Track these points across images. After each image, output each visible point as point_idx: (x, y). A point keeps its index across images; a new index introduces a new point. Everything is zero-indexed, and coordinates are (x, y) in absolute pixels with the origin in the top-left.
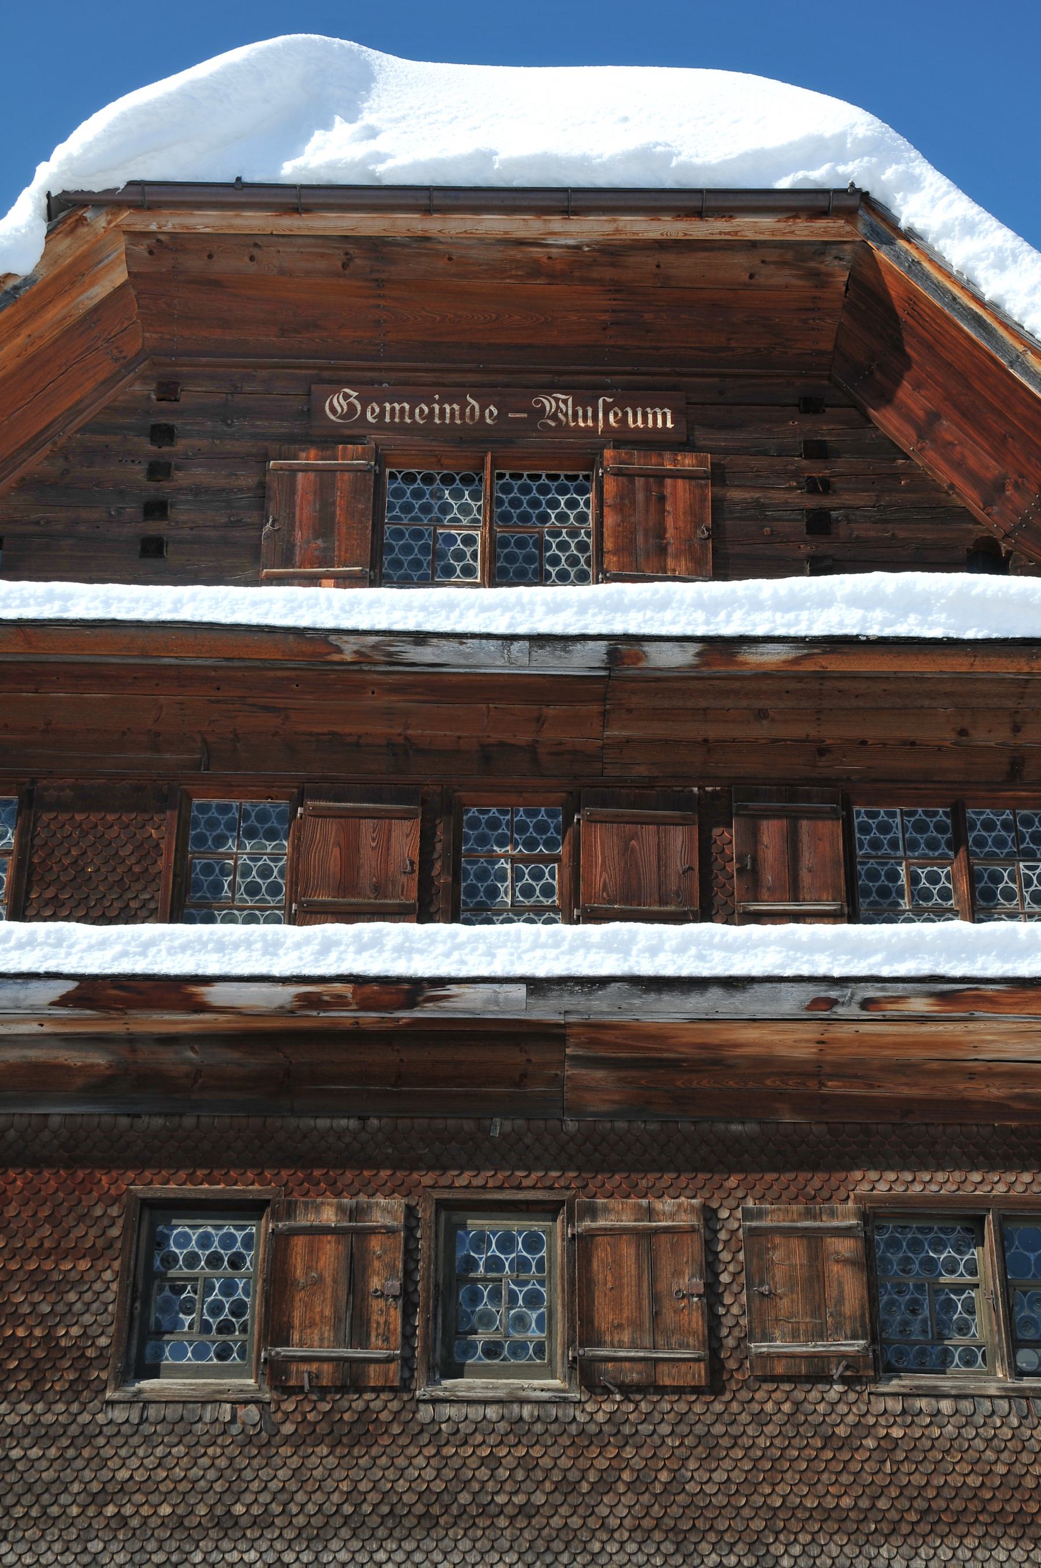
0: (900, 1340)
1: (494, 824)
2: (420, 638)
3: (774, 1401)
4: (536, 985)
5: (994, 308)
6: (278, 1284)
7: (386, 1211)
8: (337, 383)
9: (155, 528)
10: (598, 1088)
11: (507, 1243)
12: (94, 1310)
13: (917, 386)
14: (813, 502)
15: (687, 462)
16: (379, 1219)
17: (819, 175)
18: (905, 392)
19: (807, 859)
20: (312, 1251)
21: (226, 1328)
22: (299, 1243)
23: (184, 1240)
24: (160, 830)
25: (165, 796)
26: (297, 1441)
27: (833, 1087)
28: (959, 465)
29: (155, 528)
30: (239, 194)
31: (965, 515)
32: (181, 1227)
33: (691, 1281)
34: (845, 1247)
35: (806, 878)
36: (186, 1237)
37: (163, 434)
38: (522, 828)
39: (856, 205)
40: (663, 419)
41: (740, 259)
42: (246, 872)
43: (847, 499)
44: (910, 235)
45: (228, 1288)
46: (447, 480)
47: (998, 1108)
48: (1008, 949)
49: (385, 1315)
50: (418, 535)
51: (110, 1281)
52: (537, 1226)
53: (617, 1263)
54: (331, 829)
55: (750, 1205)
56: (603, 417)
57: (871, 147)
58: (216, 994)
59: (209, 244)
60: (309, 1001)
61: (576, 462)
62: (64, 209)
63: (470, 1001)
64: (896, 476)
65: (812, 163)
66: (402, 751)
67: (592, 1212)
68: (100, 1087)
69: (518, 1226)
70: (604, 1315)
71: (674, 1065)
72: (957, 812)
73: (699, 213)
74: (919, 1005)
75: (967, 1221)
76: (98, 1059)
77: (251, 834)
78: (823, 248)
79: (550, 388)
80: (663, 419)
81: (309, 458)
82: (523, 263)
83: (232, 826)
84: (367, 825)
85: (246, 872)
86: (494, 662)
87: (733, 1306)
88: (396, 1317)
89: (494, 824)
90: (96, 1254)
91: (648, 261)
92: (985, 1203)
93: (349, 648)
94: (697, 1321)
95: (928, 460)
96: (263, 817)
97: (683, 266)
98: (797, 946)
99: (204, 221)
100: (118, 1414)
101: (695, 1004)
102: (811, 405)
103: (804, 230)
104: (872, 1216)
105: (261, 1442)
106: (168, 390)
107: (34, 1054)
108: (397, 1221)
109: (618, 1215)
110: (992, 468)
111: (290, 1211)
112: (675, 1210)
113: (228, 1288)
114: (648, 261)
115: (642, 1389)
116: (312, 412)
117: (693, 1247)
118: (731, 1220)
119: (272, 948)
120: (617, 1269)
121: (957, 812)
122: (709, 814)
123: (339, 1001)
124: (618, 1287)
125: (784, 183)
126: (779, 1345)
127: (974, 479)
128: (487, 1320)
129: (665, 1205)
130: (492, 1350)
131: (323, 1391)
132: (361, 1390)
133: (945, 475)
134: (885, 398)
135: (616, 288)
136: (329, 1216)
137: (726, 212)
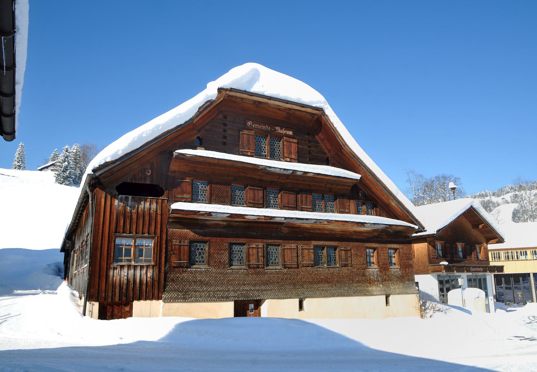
0: (316, 262)
1: (270, 192)
2: (270, 167)
3: (304, 269)
4: (285, 218)
5: (335, 128)
6: (248, 255)
7: (261, 245)
8: (249, 120)
9: (225, 140)
10: (285, 230)
11: (273, 250)
12: (225, 257)
13: (322, 134)
14: (308, 149)
15: (295, 141)
16: (260, 246)
17: (318, 105)
18: (320, 134)
19: (308, 200)
20: (252, 250)
21: (241, 260)
22: (251, 249)
23: (235, 248)
24: (228, 189)
25: (228, 184)
26: (251, 274)
27: (311, 231)
28: (326, 147)
29: (225, 140)
30: (245, 92)
31: (326, 153)
32: (234, 246)
33: (295, 255)
34: (312, 251)
35: (308, 203)
36: (236, 248)
37: (225, 125)
38: (273, 192)
39: (321, 110)
40: (291, 133)
41: (305, 113)
42: (239, 196)
43: (312, 149)
44: (326, 115)
45: (241, 255)
46: (262, 137)
47: (327, 234)
48: (335, 217)
49: (261, 259)
50: (258, 146)
51: (227, 253)
52: (277, 247)
53: (287, 253)
54: (251, 192)
55: (301, 245)
56: (283, 131)
57: (324, 103)
58: (247, 217)
59: (236, 97)
60: (259, 219)
61: (280, 137)
62: (220, 90)
63: (277, 220)
64: (318, 146)
65: (317, 103)
66: (261, 181)
67: (284, 246)
68: (224, 227)
69: (275, 247)
70: (286, 259)
71: (295, 228)
72: (323, 195)
73: (303, 107)
74: (325, 223)
75: (323, 248)
76: (225, 223)
77: (239, 190)
78: (315, 114)
79: (277, 126)
80: (291, 133)
81: (246, 132)
82: (279, 109)
83: (237, 189)
84: (256, 191)
85: (239, 196)
86: (278, 171)
87: (300, 258)
88: (262, 259)
89: (270, 192)
90: (225, 250)
91: (294, 111)
92: (325, 246)
93: (261, 167)
94: (296, 260)
95: (322, 145)
96: (241, 188)
97: (297, 113)
98: (314, 215)
99: (238, 95)
100: (229, 271)
101: (302, 221)
102: (309, 134)
103: (314, 112)
104: (316, 247)
105: (247, 275)
106: (225, 117)
107: (217, 222)
108: (262, 247)
109: (288, 246)
110: (330, 147)
111: (249, 245)
112: (293, 246)
113: (241, 255)
114: (294, 111)
115: (290, 268)
116: (245, 124)
117: (296, 250)
118: (300, 247)
119: (255, 211)
120: (253, 252)
121: (323, 195)
122: (297, 193)
123: (262, 219)
124: (184, 255)
125: (314, 106)
126: (305, 263)
127: (327, 149)
128: (271, 259)
129: (292, 245)
130: (272, 263)
131: (254, 268)
132: (258, 268)
133: (324, 148)
134: (317, 134)
135: (288, 113)
136: (254, 246)
137: (305, 107)
